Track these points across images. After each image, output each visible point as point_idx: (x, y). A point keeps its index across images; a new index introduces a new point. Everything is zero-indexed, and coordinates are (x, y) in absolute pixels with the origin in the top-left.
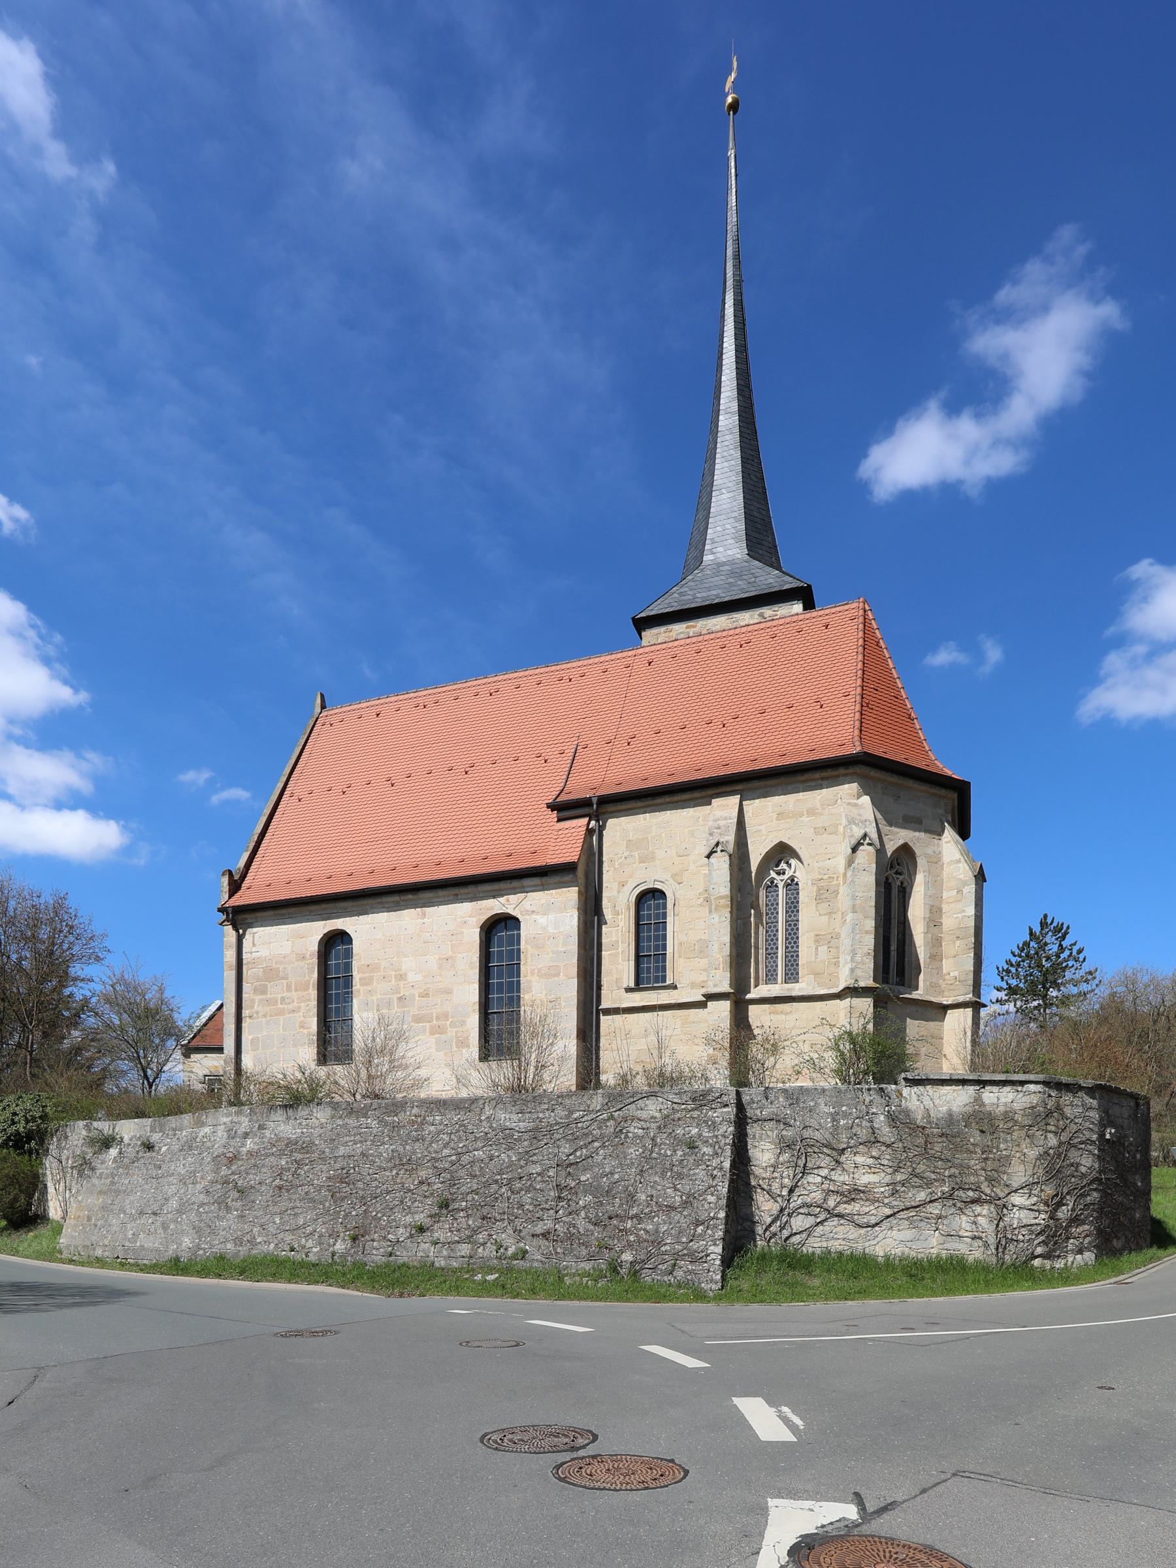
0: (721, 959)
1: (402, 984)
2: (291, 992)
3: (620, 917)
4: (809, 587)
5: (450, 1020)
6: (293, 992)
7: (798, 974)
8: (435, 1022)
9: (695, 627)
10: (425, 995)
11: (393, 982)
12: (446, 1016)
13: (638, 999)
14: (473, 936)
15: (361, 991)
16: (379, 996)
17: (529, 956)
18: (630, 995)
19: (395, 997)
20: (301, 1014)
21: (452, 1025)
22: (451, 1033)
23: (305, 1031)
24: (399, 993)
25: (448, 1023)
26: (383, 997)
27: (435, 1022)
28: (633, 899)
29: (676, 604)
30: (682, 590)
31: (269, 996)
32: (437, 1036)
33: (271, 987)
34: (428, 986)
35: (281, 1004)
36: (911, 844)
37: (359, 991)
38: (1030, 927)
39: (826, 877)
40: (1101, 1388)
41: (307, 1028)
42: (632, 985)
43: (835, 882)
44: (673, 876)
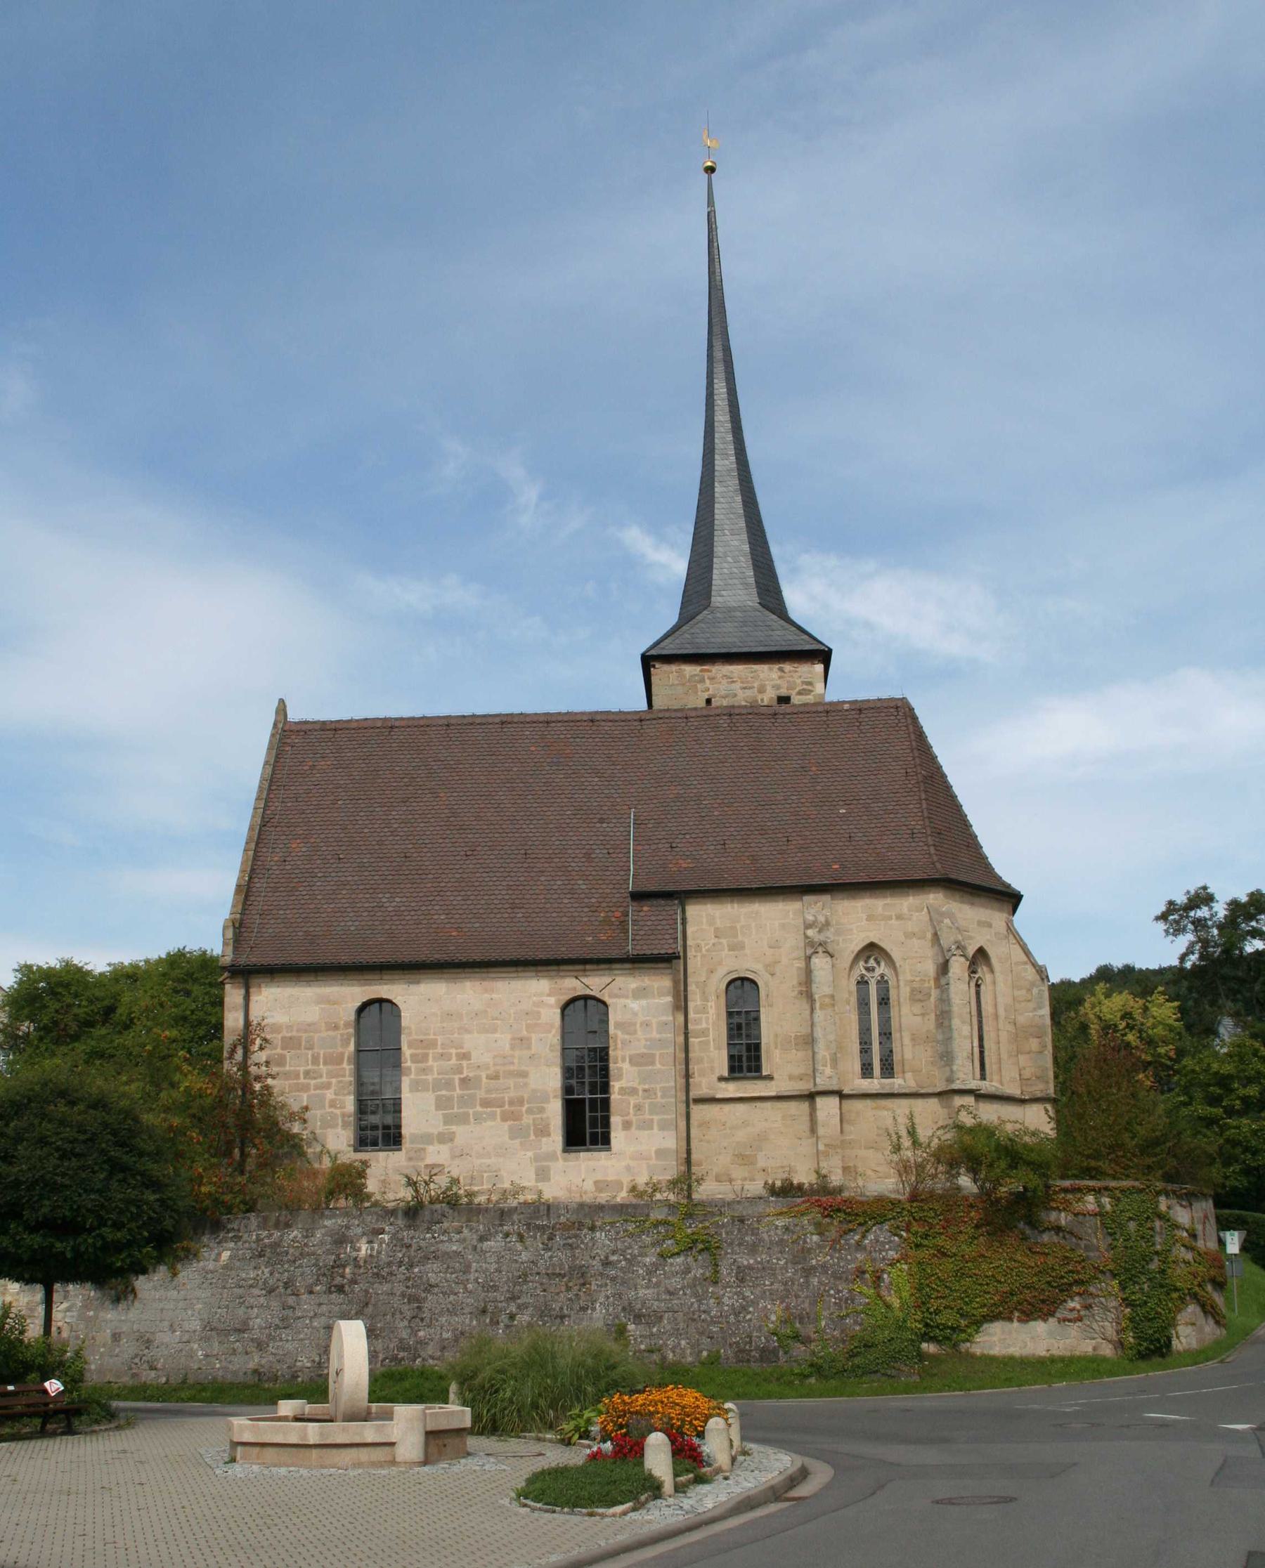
0: (828, 1057)
1: (465, 1063)
2: (319, 1065)
3: (709, 1004)
4: (830, 651)
5: (526, 1106)
6: (321, 1066)
7: (892, 1069)
8: (507, 1107)
9: (710, 671)
10: (495, 1077)
11: (454, 1061)
12: (521, 1101)
13: (731, 1090)
14: (552, 1016)
15: (413, 1070)
16: (436, 1076)
17: (619, 1042)
18: (723, 1085)
19: (457, 1077)
20: (332, 1091)
21: (529, 1111)
22: (527, 1120)
23: (338, 1112)
24: (462, 1073)
25: (524, 1109)
26: (440, 1077)
27: (507, 1107)
28: (723, 986)
29: (688, 646)
30: (692, 631)
31: (287, 1068)
32: (509, 1123)
33: (291, 1058)
34: (498, 1068)
35: (305, 1078)
36: (985, 947)
37: (409, 1069)
38: (282, 701)
39: (918, 979)
40: (1012, 1500)
41: (341, 1108)
42: (726, 1074)
43: (926, 985)
44: (767, 966)
